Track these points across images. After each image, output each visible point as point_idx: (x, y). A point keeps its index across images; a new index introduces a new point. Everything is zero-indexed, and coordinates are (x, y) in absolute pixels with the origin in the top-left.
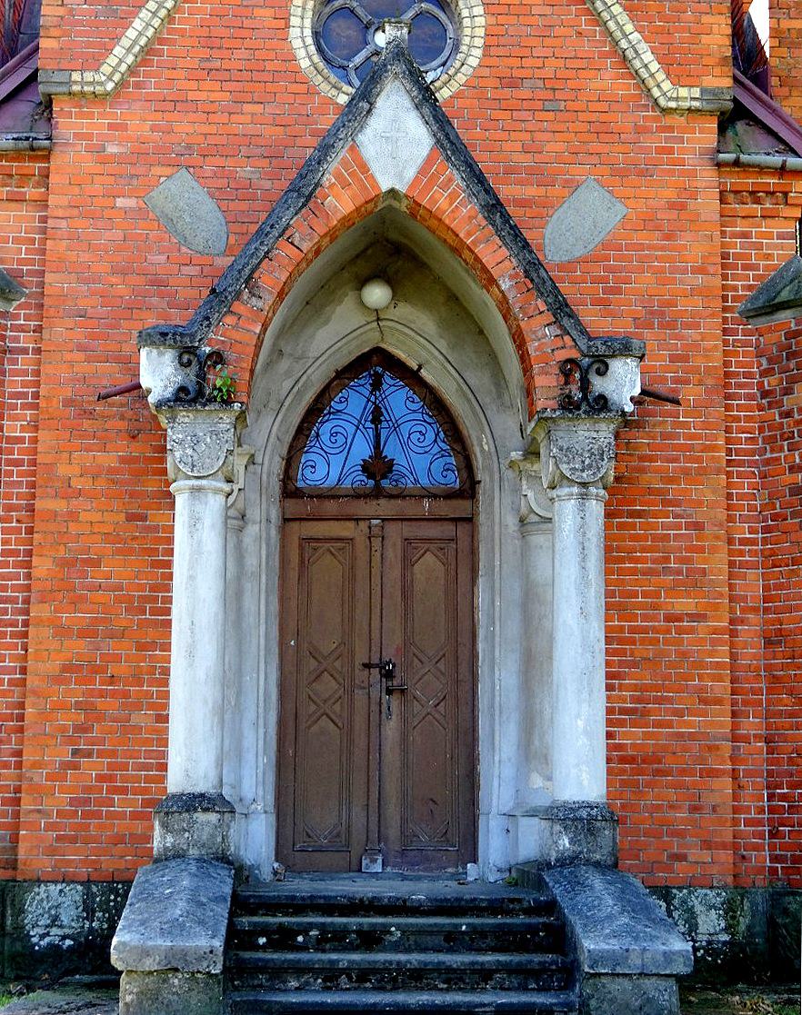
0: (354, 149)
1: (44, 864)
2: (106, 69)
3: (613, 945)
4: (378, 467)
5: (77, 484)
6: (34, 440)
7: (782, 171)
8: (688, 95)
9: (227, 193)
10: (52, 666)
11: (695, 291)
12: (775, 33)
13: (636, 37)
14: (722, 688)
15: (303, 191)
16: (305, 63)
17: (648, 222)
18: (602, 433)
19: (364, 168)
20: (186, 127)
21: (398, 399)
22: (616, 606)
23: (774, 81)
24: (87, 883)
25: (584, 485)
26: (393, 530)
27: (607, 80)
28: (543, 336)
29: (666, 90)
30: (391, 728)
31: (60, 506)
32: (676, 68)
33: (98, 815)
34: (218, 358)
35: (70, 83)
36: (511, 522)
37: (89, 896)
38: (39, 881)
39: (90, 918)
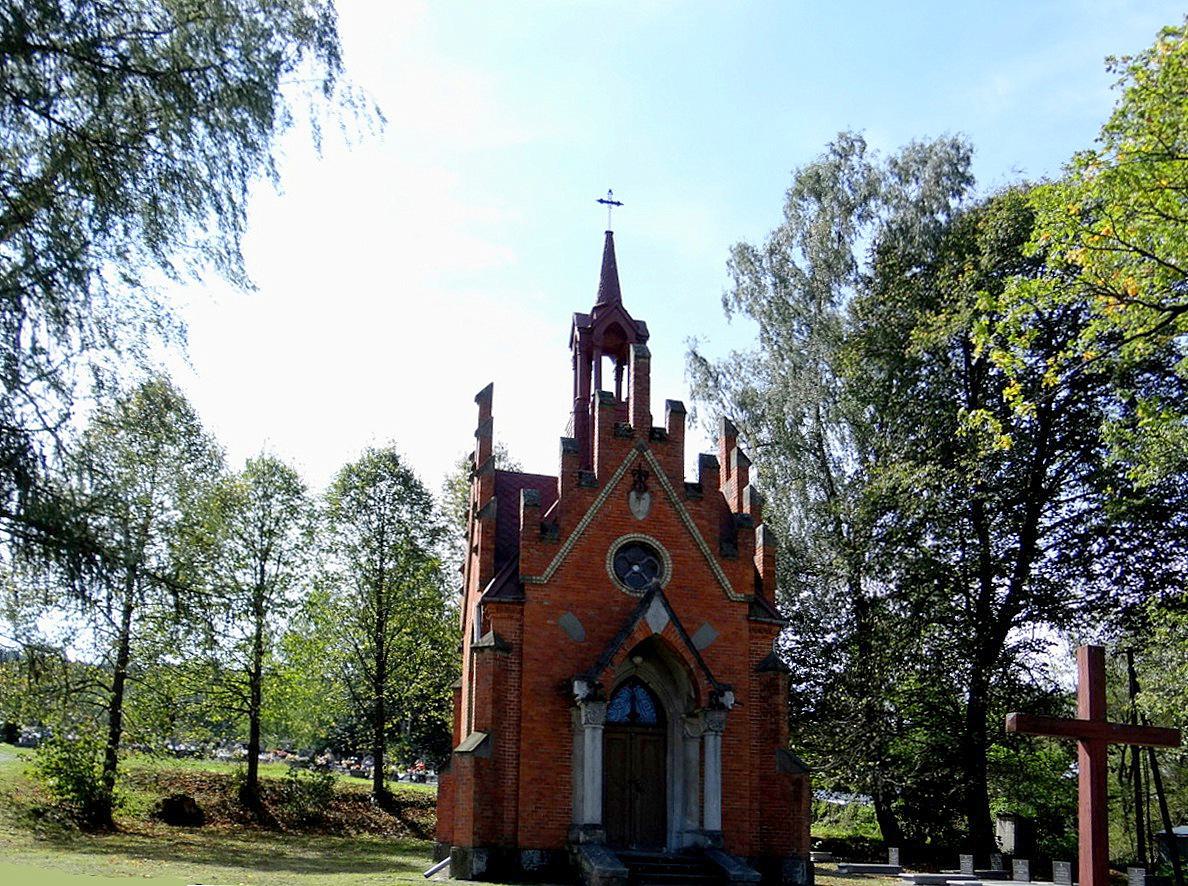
0: (644, 618)
1: (526, 844)
2: (545, 576)
3: (739, 873)
4: (634, 715)
5: (535, 718)
6: (520, 702)
7: (770, 624)
8: (740, 596)
9: (585, 620)
10: (527, 779)
11: (741, 662)
12: (764, 572)
13: (723, 575)
14: (747, 794)
15: (626, 628)
16: (611, 577)
17: (725, 639)
18: (722, 716)
19: (647, 625)
20: (570, 597)
21: (640, 692)
22: (724, 766)
23: (764, 588)
24: (541, 850)
25: (716, 732)
26: (639, 738)
27: (713, 589)
28: (703, 683)
29: (732, 593)
30: (638, 803)
31: (530, 726)
32: (737, 587)
33: (544, 828)
34: (601, 686)
35: (532, 579)
36: (680, 736)
37: (542, 855)
38: (525, 849)
39: (543, 861)
